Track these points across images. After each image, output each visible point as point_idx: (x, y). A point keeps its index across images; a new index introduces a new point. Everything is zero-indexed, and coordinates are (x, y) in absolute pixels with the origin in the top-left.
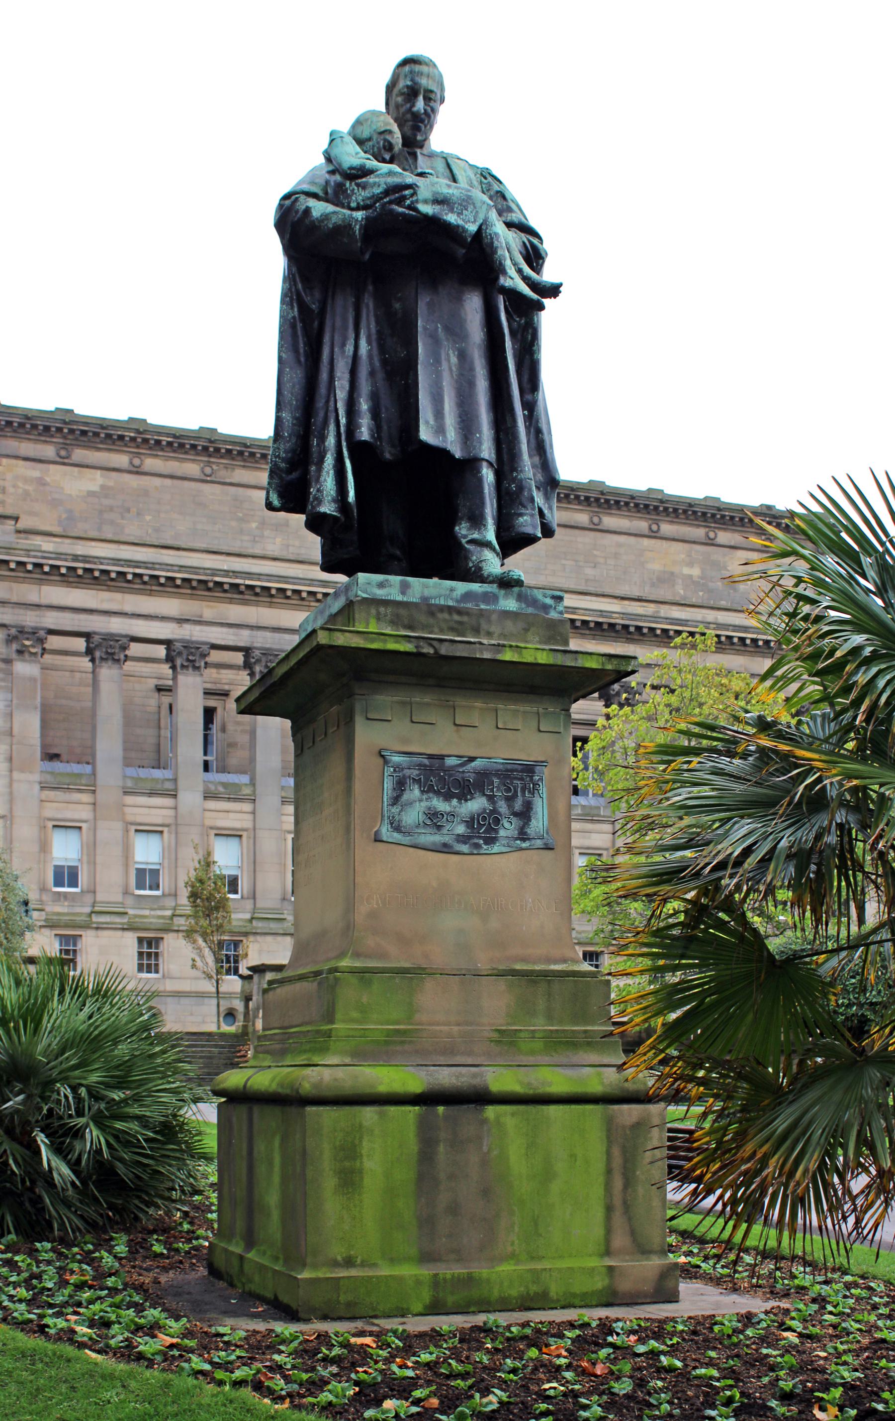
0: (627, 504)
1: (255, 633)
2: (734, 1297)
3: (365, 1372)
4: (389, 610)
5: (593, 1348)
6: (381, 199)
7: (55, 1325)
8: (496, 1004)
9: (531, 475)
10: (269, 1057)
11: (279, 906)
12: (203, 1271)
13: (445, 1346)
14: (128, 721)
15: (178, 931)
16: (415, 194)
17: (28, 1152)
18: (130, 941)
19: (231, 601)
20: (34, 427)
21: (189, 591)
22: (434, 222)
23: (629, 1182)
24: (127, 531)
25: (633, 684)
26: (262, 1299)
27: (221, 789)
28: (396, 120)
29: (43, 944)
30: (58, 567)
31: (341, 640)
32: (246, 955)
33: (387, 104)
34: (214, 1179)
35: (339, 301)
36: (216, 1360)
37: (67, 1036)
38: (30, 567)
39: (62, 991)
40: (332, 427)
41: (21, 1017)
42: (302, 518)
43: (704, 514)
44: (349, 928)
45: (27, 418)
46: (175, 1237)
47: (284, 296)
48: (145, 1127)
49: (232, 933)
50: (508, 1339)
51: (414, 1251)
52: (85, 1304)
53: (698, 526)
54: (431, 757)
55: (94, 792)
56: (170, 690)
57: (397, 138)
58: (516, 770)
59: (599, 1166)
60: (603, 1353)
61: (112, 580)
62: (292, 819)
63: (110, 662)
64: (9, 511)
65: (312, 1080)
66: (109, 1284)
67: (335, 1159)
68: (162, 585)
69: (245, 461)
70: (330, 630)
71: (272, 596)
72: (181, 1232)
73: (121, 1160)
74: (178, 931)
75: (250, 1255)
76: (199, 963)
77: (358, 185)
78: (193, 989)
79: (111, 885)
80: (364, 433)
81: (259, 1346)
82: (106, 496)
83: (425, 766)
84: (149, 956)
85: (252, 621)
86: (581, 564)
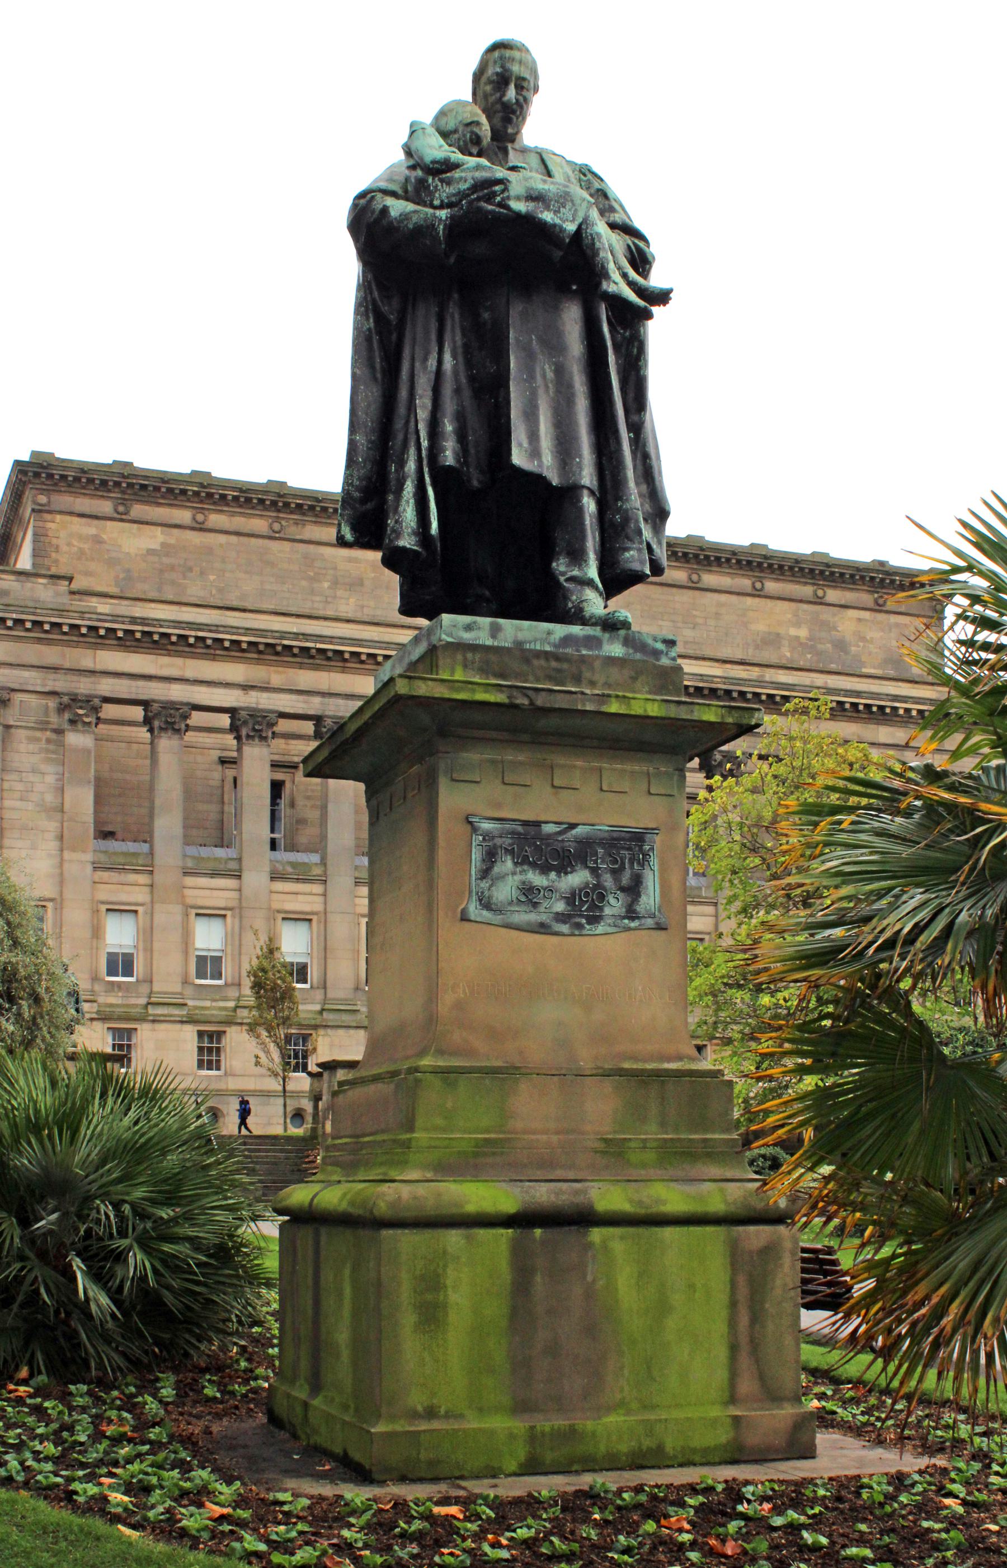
0: (728, 560)
1: (326, 700)
2: (879, 1452)
3: (451, 1554)
4: (478, 656)
5: (720, 1519)
6: (469, 195)
7: (85, 1492)
8: (600, 1109)
9: (638, 504)
10: (339, 1170)
11: (351, 996)
12: (262, 1418)
13: (544, 1516)
14: (189, 795)
15: (241, 1024)
16: (506, 189)
17: (62, 1279)
18: (190, 1033)
19: (301, 666)
20: (91, 481)
21: (255, 656)
22: (528, 220)
23: (756, 1318)
24: (189, 591)
25: (739, 753)
26: (327, 1454)
27: (290, 869)
28: (484, 111)
29: (95, 1038)
30: (114, 630)
31: (423, 689)
32: (315, 1049)
33: (474, 94)
34: (275, 1306)
35: (421, 312)
36: (274, 1537)
37: (108, 1145)
38: (84, 631)
39: (104, 1095)
40: (412, 451)
41: (56, 1123)
42: (378, 555)
43: (812, 571)
44: (431, 1019)
45: (83, 471)
46: (230, 1377)
47: (358, 305)
48: (197, 1249)
49: (301, 1026)
50: (619, 1508)
51: (506, 1400)
52: (122, 1462)
53: (806, 583)
54: (525, 823)
55: (151, 872)
56: (235, 763)
57: (485, 130)
58: (623, 839)
59: (721, 1297)
60: (733, 1526)
61: (173, 643)
62: (366, 901)
63: (170, 732)
64: (62, 571)
65: (387, 1198)
66: (152, 1436)
67: (415, 1292)
68: (226, 649)
69: (316, 516)
70: (410, 678)
71: (345, 660)
72: (237, 1371)
73: (169, 1288)
74: (241, 1024)
75: (316, 1402)
76: (264, 1059)
77: (442, 181)
78: (258, 1088)
79: (168, 974)
80: (449, 457)
81: (327, 1516)
82: (167, 555)
83: (519, 834)
84: (210, 1053)
85: (324, 687)
86: (680, 625)
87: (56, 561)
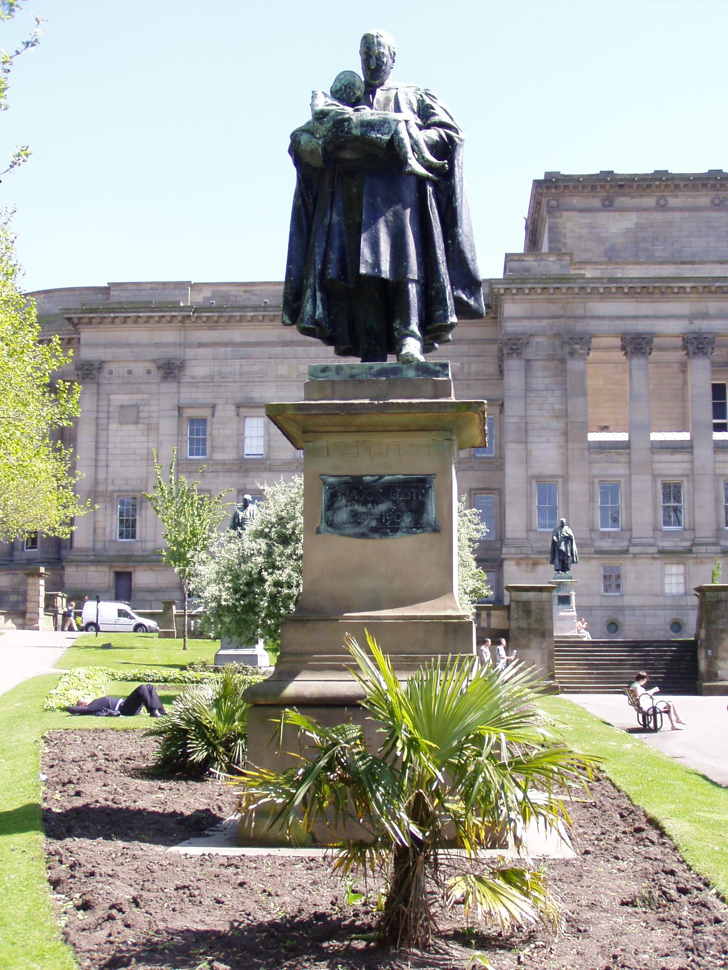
87: (565, 244)
